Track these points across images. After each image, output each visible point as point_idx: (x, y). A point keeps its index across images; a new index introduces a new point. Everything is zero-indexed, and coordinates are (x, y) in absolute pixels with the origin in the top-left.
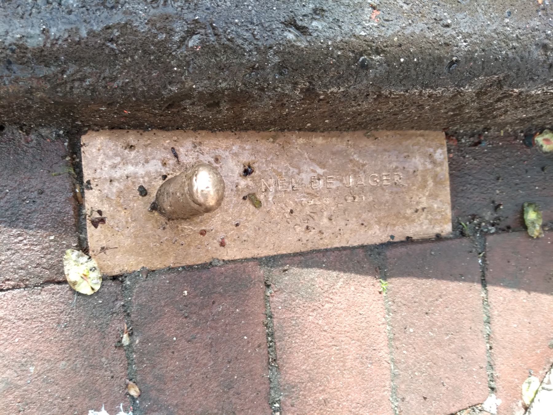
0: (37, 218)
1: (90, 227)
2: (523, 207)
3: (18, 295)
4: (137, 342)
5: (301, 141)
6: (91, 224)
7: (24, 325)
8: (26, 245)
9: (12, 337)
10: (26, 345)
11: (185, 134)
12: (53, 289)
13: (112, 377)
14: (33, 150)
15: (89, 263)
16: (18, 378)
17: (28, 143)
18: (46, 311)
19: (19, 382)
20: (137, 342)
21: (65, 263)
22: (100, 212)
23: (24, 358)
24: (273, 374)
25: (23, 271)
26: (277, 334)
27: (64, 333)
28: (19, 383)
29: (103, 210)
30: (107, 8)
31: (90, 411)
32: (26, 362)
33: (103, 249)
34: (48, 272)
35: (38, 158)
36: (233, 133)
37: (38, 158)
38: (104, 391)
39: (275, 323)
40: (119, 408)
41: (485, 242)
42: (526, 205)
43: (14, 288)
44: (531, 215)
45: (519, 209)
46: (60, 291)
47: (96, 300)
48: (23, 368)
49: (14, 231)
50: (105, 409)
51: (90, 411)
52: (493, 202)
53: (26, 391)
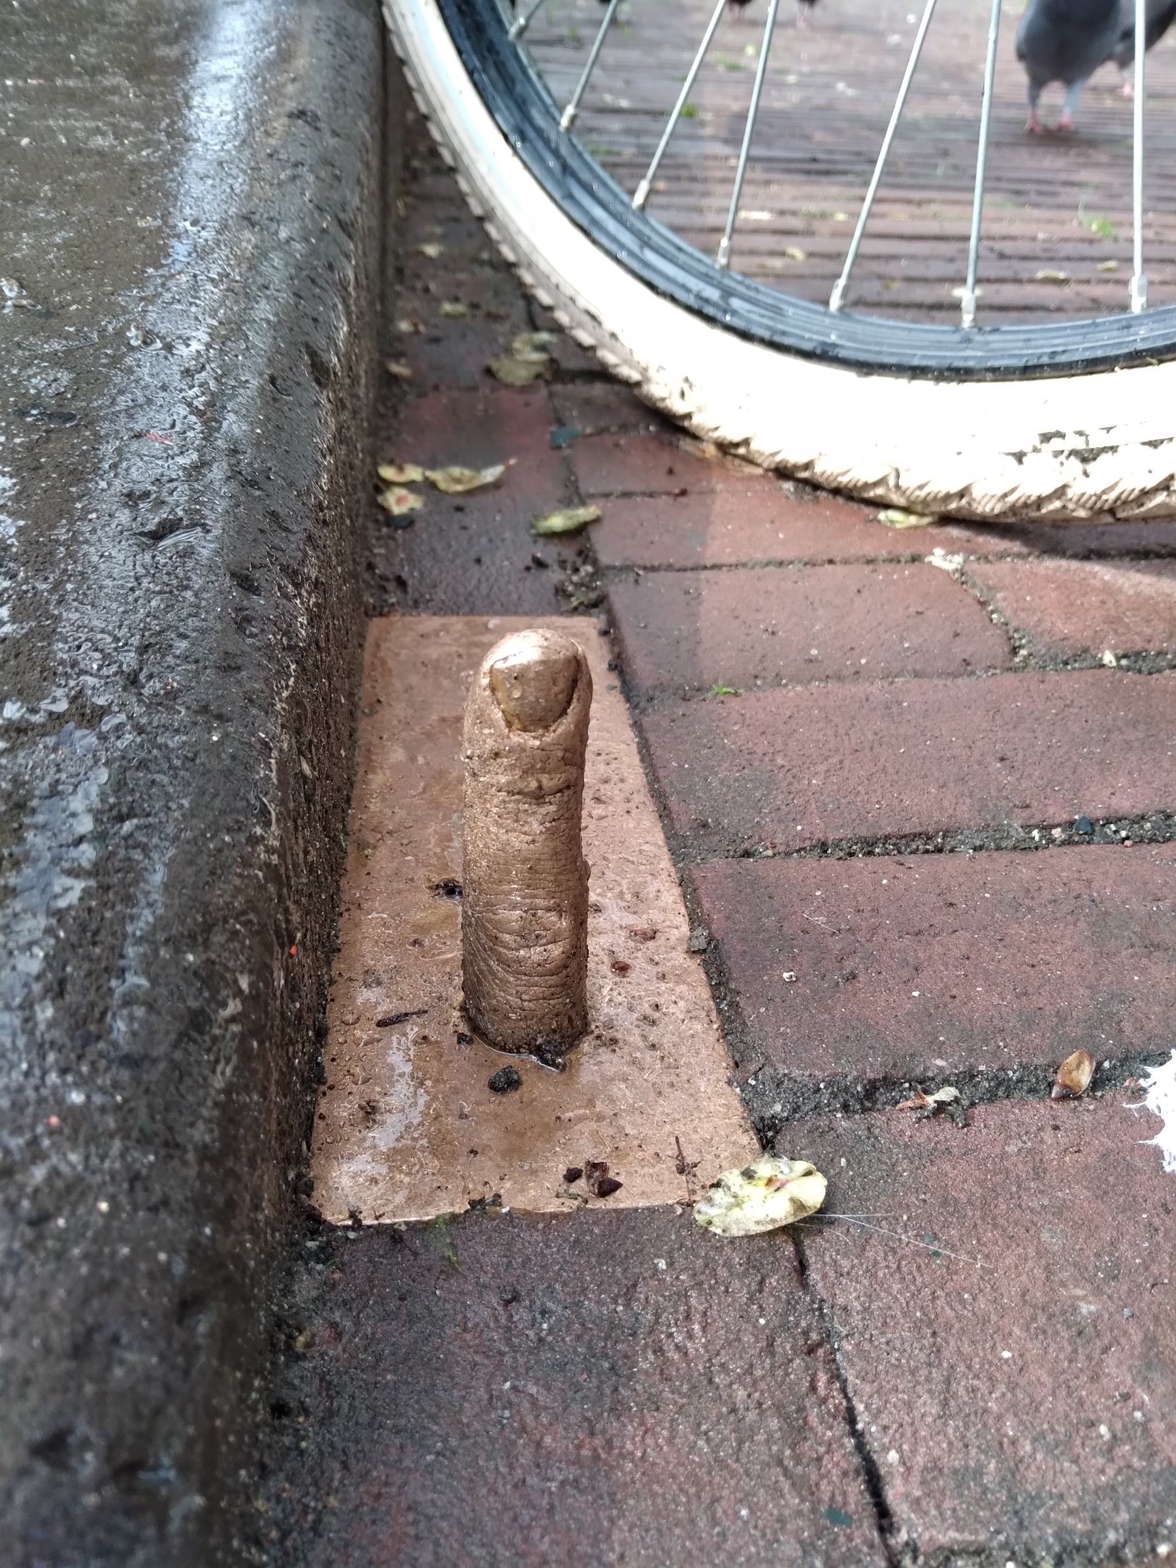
0: (599, 1302)
1: (617, 1200)
2: (540, 535)
3: (860, 1364)
4: (940, 1062)
5: (374, 805)
6: (610, 1198)
7: (952, 1343)
8: (690, 1336)
9: (999, 1369)
10: (1017, 1331)
11: (340, 1001)
12: (825, 1276)
13: (1056, 1128)
14: (368, 1317)
15: (730, 1183)
16: (1123, 1341)
17: (339, 1335)
18: (896, 1287)
19: (1134, 1338)
20: (940, 1062)
21: (736, 1232)
22: (572, 1176)
23: (1057, 1333)
24: (963, 843)
25: (778, 1341)
26: (864, 832)
27: (956, 1241)
28: (1137, 1338)
29: (562, 1169)
30: (138, 348)
31: (1168, 1169)
32: (1069, 1327)
33: (681, 1171)
34: (773, 1281)
35: (392, 1305)
36: (346, 915)
37: (392, 1305)
38: (1102, 1144)
39: (841, 833)
40: (1139, 1110)
41: (614, 568)
42: (533, 531)
43: (836, 1376)
44: (557, 522)
45: (541, 541)
46: (827, 1259)
47: (840, 1173)
48: (1089, 1330)
49: (646, 1362)
50: (1152, 1138)
51: (1168, 1169)
52: (528, 569)
53: (1156, 1319)
